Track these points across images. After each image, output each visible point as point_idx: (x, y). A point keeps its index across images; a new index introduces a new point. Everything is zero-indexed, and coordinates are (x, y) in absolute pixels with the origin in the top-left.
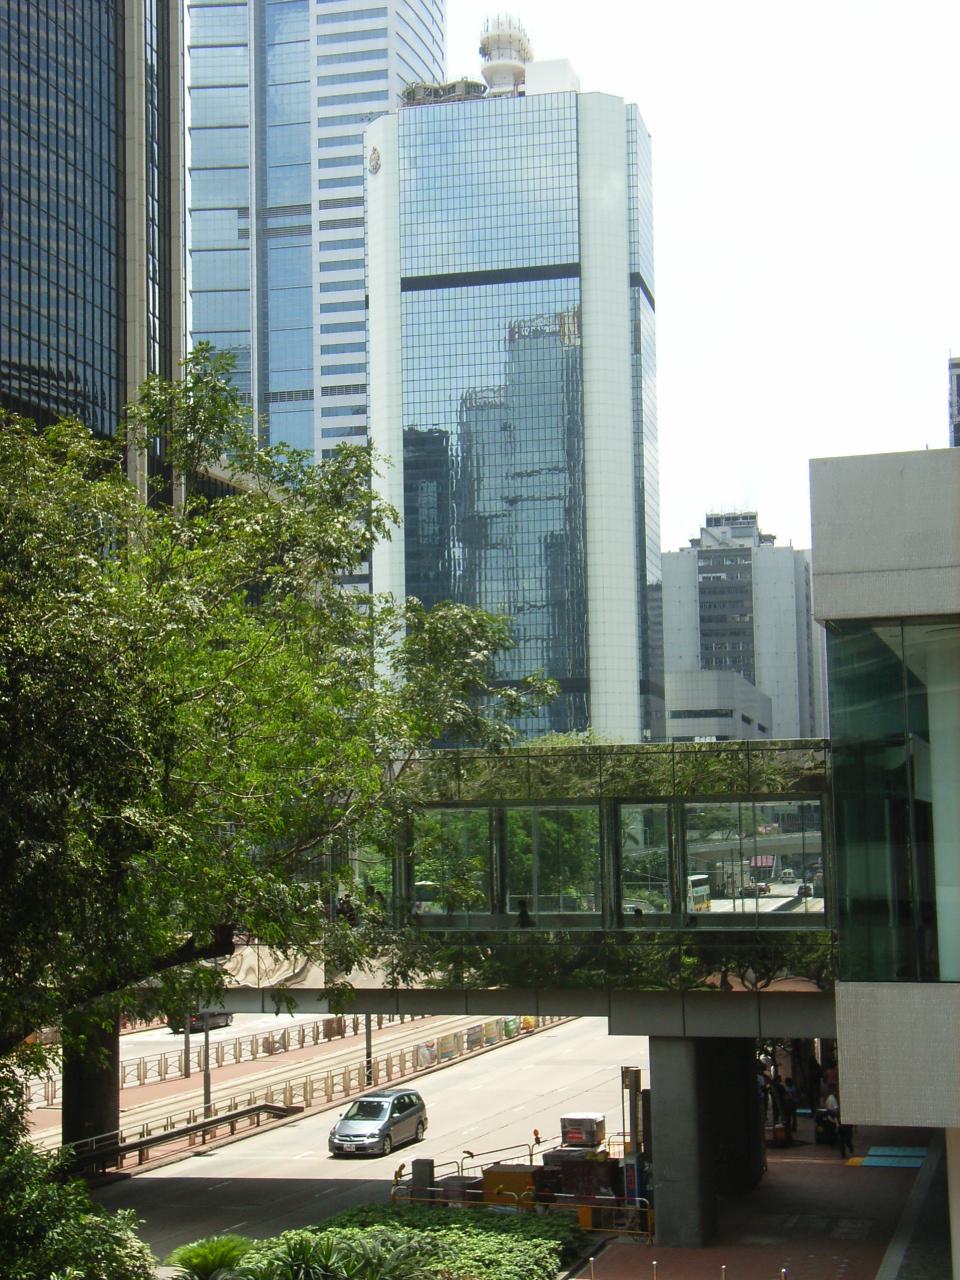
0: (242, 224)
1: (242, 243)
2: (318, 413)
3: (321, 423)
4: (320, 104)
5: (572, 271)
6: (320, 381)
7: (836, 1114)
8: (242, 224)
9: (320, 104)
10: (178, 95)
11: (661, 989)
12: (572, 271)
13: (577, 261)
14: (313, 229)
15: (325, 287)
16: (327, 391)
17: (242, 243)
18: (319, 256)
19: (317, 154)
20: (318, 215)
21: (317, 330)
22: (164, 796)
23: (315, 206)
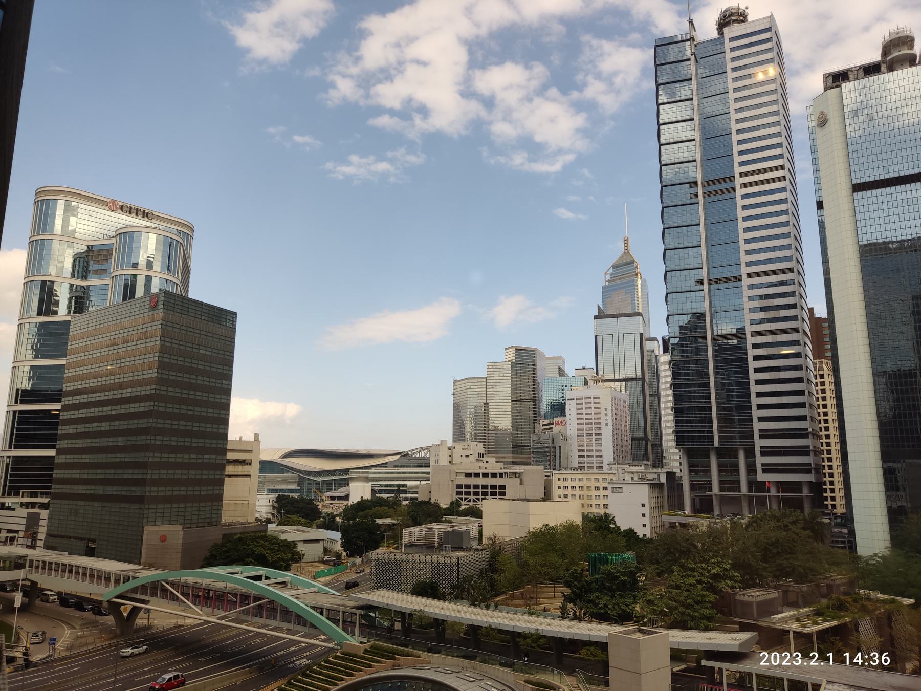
0: (693, 190)
1: (693, 201)
2: (745, 288)
3: (747, 293)
4: (741, 177)
5: (858, 188)
7: (618, 528)
8: (693, 190)
9: (741, 177)
10: (715, 378)
11: (306, 654)
12: (858, 188)
13: (855, 194)
14: (736, 177)
15: (745, 219)
16: (750, 275)
17: (693, 201)
18: (740, 202)
19: (735, 127)
20: (739, 181)
21: (742, 242)
22: (529, 582)
23: (744, 277)
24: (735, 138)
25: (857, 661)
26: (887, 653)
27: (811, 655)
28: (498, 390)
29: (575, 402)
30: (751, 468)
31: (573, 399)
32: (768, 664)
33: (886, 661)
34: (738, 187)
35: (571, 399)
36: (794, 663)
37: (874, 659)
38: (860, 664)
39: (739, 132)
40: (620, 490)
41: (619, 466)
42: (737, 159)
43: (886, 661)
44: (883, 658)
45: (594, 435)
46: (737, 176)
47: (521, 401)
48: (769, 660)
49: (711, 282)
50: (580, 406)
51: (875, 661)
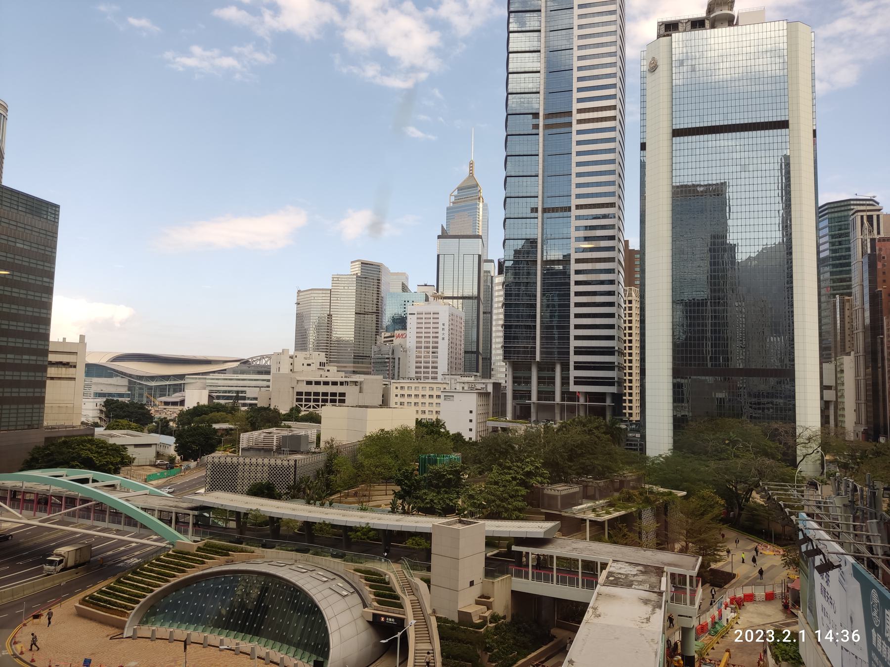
2: (573, 218)
3: (574, 223)
6: (574, 202)
8: (535, 121)
15: (579, 153)
16: (578, 207)
18: (575, 138)
19: (576, 64)
20: (576, 116)
24: (576, 74)
25: (828, 638)
26: (857, 631)
27: (784, 632)
28: (342, 302)
29: (415, 316)
30: (565, 381)
31: (414, 314)
32: (742, 641)
33: (856, 638)
34: (574, 122)
35: (412, 314)
36: (842, 640)
37: (844, 636)
38: (831, 641)
39: (580, 69)
40: (451, 398)
41: (452, 377)
42: (576, 95)
43: (856, 638)
44: (853, 635)
45: (431, 347)
46: (574, 112)
47: (365, 314)
48: (743, 638)
49: (545, 210)
50: (420, 321)
51: (846, 638)
